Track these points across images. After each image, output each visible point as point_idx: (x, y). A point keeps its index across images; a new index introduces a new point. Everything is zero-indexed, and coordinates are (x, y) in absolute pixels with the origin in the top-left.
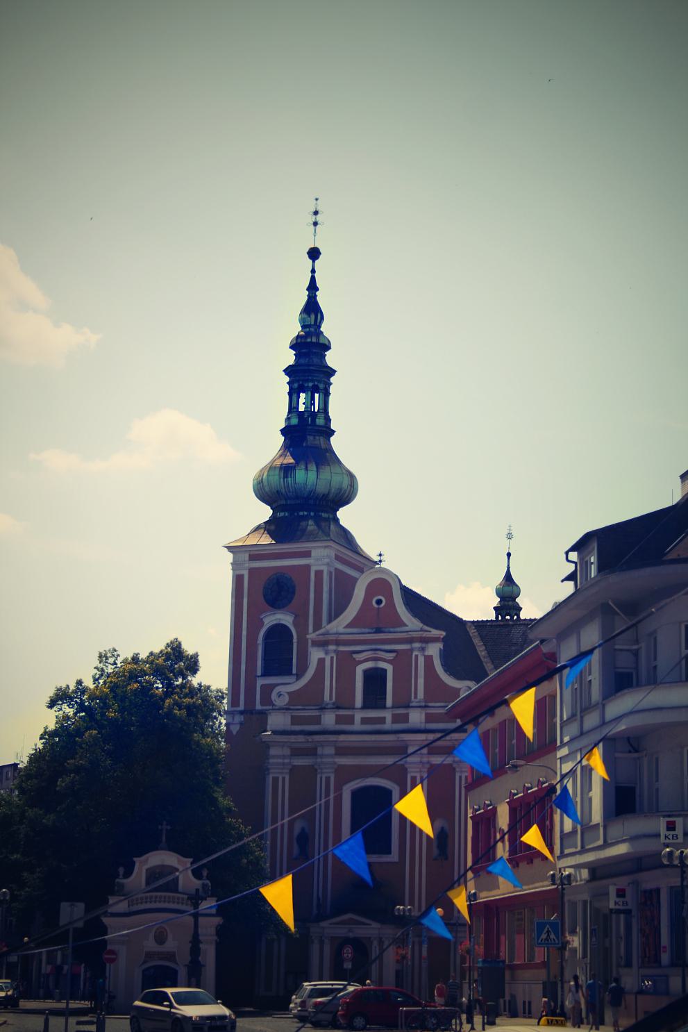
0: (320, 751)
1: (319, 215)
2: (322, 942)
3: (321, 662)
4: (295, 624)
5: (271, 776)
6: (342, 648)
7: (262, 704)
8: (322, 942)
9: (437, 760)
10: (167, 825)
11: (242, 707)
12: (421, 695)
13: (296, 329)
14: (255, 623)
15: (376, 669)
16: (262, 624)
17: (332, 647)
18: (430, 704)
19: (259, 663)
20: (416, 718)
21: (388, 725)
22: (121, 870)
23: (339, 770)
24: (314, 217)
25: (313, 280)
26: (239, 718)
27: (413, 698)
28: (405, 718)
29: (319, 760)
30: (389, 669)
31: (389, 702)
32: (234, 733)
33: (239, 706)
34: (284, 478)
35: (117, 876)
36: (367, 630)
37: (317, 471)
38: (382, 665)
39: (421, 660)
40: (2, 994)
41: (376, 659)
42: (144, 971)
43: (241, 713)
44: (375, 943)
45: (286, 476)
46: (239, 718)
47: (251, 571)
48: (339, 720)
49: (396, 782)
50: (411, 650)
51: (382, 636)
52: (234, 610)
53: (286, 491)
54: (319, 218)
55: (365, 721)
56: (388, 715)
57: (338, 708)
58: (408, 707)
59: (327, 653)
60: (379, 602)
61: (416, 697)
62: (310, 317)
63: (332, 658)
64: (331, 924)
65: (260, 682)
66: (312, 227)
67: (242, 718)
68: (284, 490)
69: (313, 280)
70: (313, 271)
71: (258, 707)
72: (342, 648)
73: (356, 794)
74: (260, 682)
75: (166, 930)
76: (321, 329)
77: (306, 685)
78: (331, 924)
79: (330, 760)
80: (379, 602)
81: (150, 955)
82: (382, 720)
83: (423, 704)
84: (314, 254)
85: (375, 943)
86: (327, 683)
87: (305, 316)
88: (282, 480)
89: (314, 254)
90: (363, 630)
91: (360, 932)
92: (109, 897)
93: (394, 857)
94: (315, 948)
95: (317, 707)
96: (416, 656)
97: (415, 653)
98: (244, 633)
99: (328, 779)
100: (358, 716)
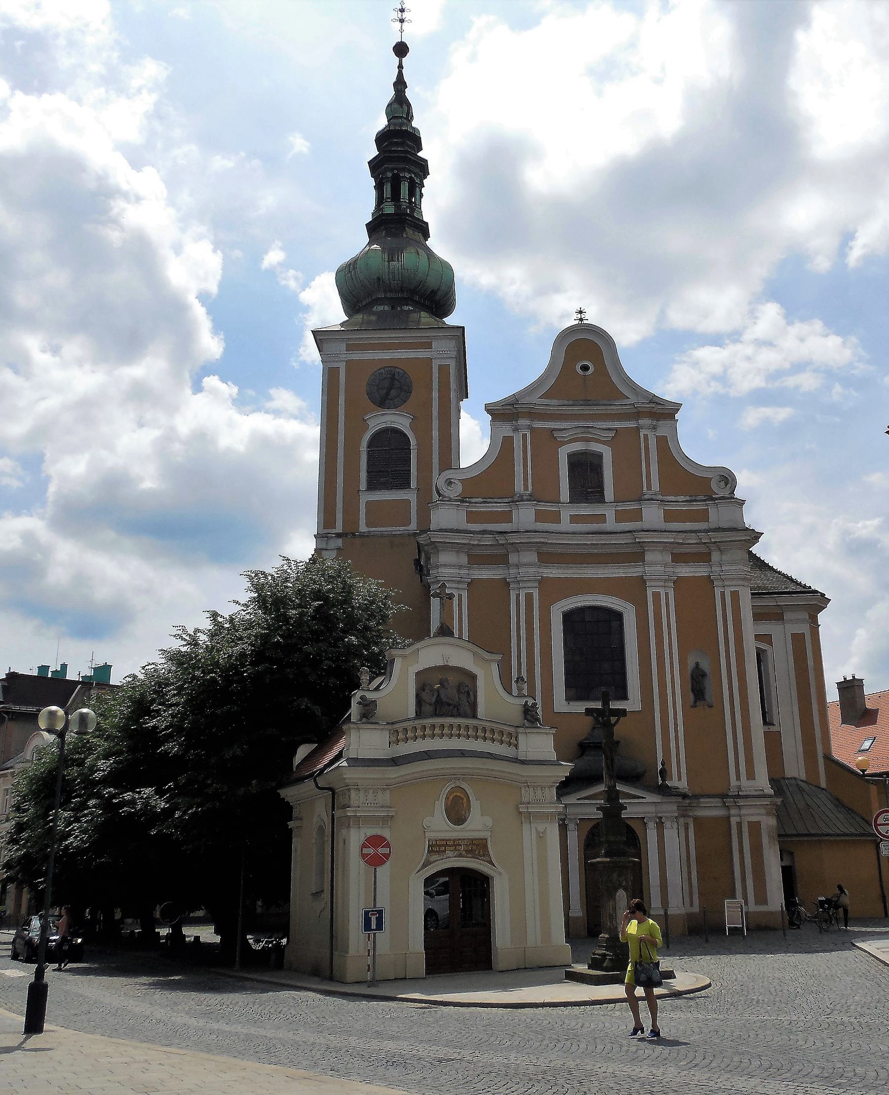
0: (513, 558)
1: (405, 12)
4: (412, 427)
6: (538, 425)
7: (367, 525)
9: (686, 571)
11: (339, 529)
12: (656, 486)
13: (382, 122)
14: (356, 425)
16: (367, 427)
17: (523, 422)
19: (363, 475)
20: (653, 515)
21: (611, 524)
23: (543, 582)
24: (400, 13)
25: (400, 75)
27: (645, 489)
28: (637, 515)
29: (513, 571)
31: (609, 492)
34: (388, 262)
36: (566, 402)
38: (595, 447)
39: (653, 442)
41: (588, 440)
43: (339, 535)
47: (349, 363)
48: (540, 516)
50: (638, 429)
51: (595, 410)
52: (325, 420)
53: (389, 279)
54: (405, 15)
55: (574, 519)
56: (610, 513)
58: (640, 500)
59: (516, 430)
60: (585, 368)
61: (649, 487)
63: (525, 436)
64: (643, 798)
65: (366, 498)
67: (339, 542)
69: (400, 75)
70: (400, 67)
71: (363, 528)
72: (538, 425)
73: (569, 618)
76: (414, 124)
78: (643, 798)
79: (532, 570)
80: (585, 368)
81: (437, 847)
82: (602, 518)
84: (401, 50)
86: (519, 469)
87: (396, 106)
89: (401, 50)
90: (566, 402)
95: (507, 500)
96: (646, 436)
97: (642, 433)
98: (341, 437)
99: (529, 597)
100: (565, 515)
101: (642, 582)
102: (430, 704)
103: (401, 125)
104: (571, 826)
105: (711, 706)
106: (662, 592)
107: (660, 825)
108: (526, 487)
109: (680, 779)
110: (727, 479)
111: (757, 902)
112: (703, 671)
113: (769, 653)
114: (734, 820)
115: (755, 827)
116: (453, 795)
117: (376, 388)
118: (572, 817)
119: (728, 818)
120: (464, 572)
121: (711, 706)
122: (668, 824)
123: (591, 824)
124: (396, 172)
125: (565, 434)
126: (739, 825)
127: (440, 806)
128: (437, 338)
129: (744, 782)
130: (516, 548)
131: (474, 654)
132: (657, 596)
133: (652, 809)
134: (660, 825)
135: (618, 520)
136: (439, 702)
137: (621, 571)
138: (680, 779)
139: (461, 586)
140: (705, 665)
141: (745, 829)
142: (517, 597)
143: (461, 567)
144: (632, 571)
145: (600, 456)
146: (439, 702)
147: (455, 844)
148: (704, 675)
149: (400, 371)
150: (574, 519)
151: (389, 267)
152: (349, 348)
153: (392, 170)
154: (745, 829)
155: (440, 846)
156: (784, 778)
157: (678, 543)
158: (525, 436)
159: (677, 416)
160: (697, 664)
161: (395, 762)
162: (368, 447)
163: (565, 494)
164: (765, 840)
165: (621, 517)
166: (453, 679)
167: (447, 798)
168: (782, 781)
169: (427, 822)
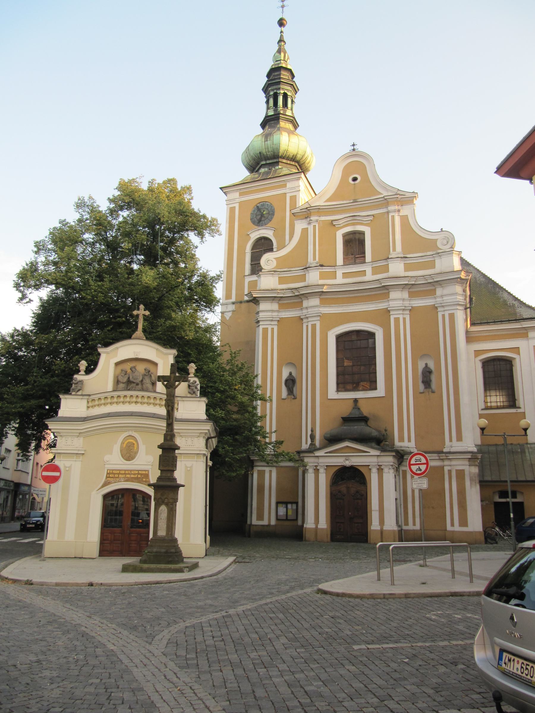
2: (317, 471)
3: (305, 231)
4: (274, 235)
5: (261, 327)
8: (317, 471)
10: (138, 309)
11: (233, 299)
15: (354, 233)
18: (408, 256)
22: (83, 365)
23: (322, 317)
26: (232, 307)
28: (386, 269)
29: (305, 311)
30: (367, 231)
31: (368, 256)
32: (228, 318)
33: (231, 298)
35: (78, 371)
37: (289, 137)
38: (359, 228)
40: (1, 548)
41: (353, 224)
42: (106, 497)
43: (233, 303)
44: (374, 471)
45: (266, 140)
46: (232, 307)
47: (240, 203)
49: (381, 325)
53: (266, 152)
56: (368, 269)
57: (322, 266)
59: (309, 224)
61: (394, 250)
62: (280, 54)
63: (315, 226)
64: (330, 452)
66: (281, 9)
68: (264, 151)
73: (340, 338)
74: (247, 280)
75: (137, 441)
77: (292, 252)
78: (330, 452)
81: (112, 475)
82: (364, 273)
83: (402, 256)
85: (374, 471)
88: (263, 143)
89: (281, 23)
91: (355, 461)
92: (61, 396)
93: (380, 391)
94: (310, 477)
97: (391, 215)
99: (314, 326)
101: (387, 311)
102: (123, 383)
103: (278, 64)
104: (322, 470)
105: (433, 392)
106: (401, 317)
107: (380, 470)
108: (314, 259)
109: (409, 440)
110: (450, 239)
111: (460, 525)
112: (429, 368)
113: (517, 360)
114: (446, 469)
115: (461, 474)
116: (127, 441)
117: (255, 215)
118: (322, 464)
119: (442, 467)
120: (275, 314)
121: (433, 392)
122: (386, 470)
123: (336, 469)
124: (275, 91)
125: (341, 222)
126: (450, 472)
127: (117, 448)
128: (289, 181)
129: (454, 442)
130: (306, 296)
131: (157, 349)
132: (397, 320)
133: (375, 459)
134: (380, 470)
135: (374, 273)
136: (129, 382)
137: (373, 306)
138: (409, 440)
139: (272, 323)
140: (431, 365)
141: (454, 474)
142: (307, 326)
143: (273, 311)
144: (381, 305)
145: (362, 233)
146: (129, 382)
147: (126, 472)
148: (430, 372)
149: (269, 203)
150: (345, 275)
151: (265, 144)
152: (241, 195)
153: (273, 90)
154: (454, 474)
155: (114, 474)
156: (527, 444)
157: (413, 285)
158: (315, 226)
159: (415, 201)
160: (426, 364)
161: (84, 419)
162: (252, 249)
163: (340, 259)
164: (468, 483)
165: (375, 271)
166: (141, 368)
167: (123, 443)
168: (525, 445)
169: (107, 458)
